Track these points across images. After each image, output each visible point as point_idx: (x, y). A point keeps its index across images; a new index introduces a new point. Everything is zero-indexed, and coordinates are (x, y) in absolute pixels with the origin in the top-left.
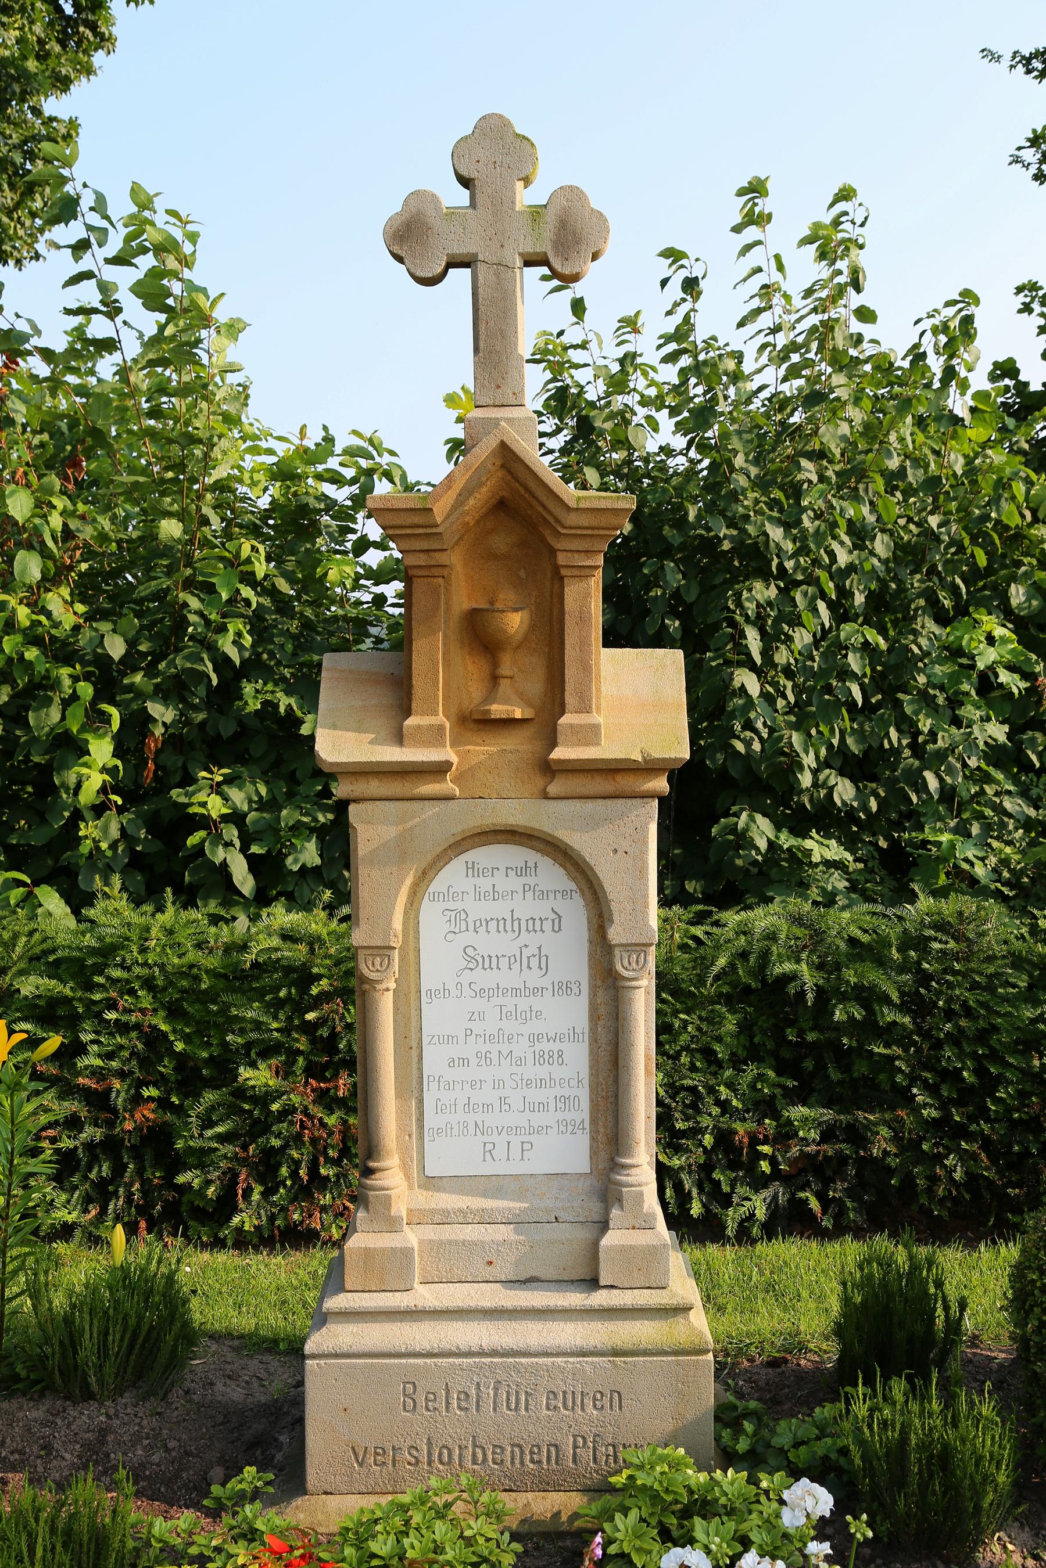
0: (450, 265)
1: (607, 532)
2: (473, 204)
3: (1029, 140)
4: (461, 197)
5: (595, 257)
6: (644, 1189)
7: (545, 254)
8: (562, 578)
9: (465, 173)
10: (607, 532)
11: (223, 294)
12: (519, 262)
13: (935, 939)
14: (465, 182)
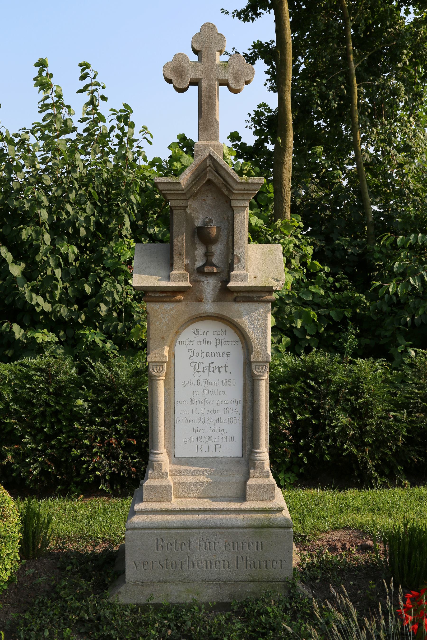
0: (191, 84)
1: (252, 192)
2: (200, 60)
3: (252, 46)
4: (195, 58)
5: (247, 83)
6: (265, 462)
7: (228, 80)
8: (233, 210)
9: (196, 48)
10: (252, 192)
11: (78, 92)
12: (217, 84)
13: (35, 375)
14: (196, 52)
